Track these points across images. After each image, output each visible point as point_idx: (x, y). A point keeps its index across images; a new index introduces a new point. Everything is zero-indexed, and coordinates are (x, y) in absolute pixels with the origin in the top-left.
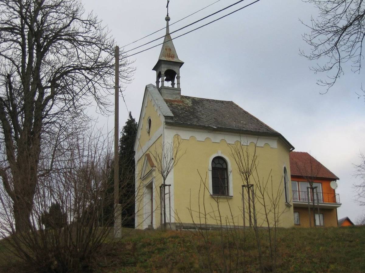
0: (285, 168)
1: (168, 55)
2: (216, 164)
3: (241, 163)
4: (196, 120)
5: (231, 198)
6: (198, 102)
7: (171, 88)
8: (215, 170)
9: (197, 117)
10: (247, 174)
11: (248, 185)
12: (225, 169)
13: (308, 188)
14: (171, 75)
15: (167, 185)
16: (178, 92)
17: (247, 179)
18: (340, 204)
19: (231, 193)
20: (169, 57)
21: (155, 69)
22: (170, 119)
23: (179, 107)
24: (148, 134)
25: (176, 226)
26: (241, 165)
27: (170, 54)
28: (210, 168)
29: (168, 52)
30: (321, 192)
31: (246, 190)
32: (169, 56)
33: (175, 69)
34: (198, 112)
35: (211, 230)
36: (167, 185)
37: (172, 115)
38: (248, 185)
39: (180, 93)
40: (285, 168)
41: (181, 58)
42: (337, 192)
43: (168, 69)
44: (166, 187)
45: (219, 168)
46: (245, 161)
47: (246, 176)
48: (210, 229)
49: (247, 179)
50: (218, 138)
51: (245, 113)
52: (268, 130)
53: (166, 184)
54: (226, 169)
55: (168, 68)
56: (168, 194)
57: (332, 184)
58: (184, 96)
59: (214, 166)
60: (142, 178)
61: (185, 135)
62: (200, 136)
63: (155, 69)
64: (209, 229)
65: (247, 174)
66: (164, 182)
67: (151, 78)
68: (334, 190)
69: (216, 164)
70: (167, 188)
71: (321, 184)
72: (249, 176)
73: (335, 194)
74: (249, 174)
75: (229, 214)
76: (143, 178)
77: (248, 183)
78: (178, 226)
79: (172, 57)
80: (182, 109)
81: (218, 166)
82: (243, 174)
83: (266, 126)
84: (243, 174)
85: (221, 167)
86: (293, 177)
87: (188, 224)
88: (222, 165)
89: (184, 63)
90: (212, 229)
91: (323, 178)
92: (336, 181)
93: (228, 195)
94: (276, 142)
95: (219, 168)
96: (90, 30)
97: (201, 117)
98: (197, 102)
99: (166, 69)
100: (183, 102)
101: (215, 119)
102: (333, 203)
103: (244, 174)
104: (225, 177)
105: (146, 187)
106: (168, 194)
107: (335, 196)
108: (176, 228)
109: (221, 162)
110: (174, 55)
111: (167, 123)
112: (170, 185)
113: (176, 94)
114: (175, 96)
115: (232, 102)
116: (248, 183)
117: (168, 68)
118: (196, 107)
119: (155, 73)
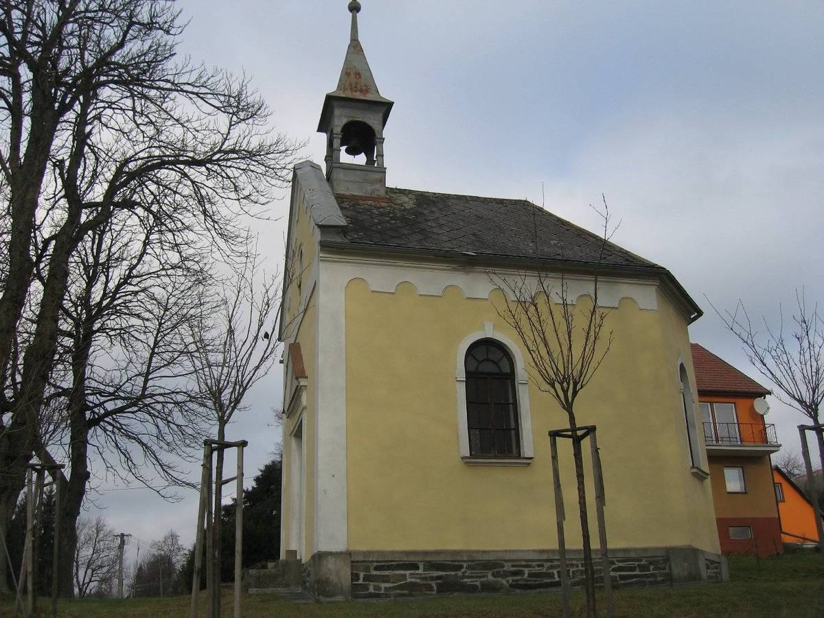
0: (682, 367)
1: (353, 86)
2: (479, 362)
3: (542, 346)
4: (419, 237)
5: (529, 464)
6: (434, 202)
7: (363, 168)
8: (473, 378)
9: (422, 231)
10: (568, 384)
11: (574, 429)
12: (506, 374)
13: (802, 429)
14: (362, 137)
15: (230, 445)
16: (377, 176)
17: (568, 407)
18: (781, 445)
19: (528, 449)
20: (355, 91)
21: (320, 129)
22: (338, 233)
23: (375, 211)
24: (298, 289)
25: (352, 562)
26: (543, 352)
27: (357, 83)
28: (462, 376)
29: (353, 79)
30: (736, 422)
31: (565, 445)
32: (354, 88)
33: (372, 120)
34: (427, 220)
35: (466, 568)
36: (230, 445)
37: (342, 222)
38: (574, 429)
39: (383, 181)
40: (682, 367)
41: (385, 93)
42: (768, 419)
43: (351, 119)
44: (226, 451)
45: (489, 374)
46: (560, 335)
47: (565, 392)
48: (465, 565)
49: (568, 407)
50: (479, 286)
51: (563, 224)
52: (627, 260)
53: (228, 438)
54: (511, 375)
55: (355, 119)
56: (234, 483)
57: (758, 404)
58: (396, 189)
59: (472, 368)
60: (286, 410)
61: (381, 277)
62: (429, 281)
63: (320, 129)
64: (461, 567)
65: (567, 386)
66: (221, 433)
67: (315, 148)
68: (762, 416)
69: (479, 362)
70: (230, 454)
71: (733, 405)
72: (575, 393)
73: (764, 424)
74: (575, 384)
75: (515, 517)
76: (288, 411)
77: (572, 419)
78: (358, 562)
79: (361, 91)
80: (381, 214)
81: (488, 368)
82: (553, 386)
83: (621, 250)
84: (553, 386)
85: (496, 370)
86: (703, 393)
87: (393, 552)
88: (496, 363)
89: (393, 103)
90: (468, 568)
91: (739, 392)
92: (764, 398)
93: (519, 456)
94: (654, 288)
95: (489, 375)
96: (172, 53)
97: (435, 230)
98: (424, 199)
99: (345, 121)
100: (390, 200)
101: (474, 235)
102: (762, 444)
103: (557, 386)
104: (508, 400)
105: (294, 436)
106: (234, 483)
107: (765, 429)
108: (352, 568)
109: (495, 355)
110: (370, 86)
111: (325, 246)
112: (243, 444)
113: (372, 182)
114: (369, 188)
115: (526, 201)
116: (572, 419)
117: (355, 119)
118: (426, 212)
119: (323, 137)
